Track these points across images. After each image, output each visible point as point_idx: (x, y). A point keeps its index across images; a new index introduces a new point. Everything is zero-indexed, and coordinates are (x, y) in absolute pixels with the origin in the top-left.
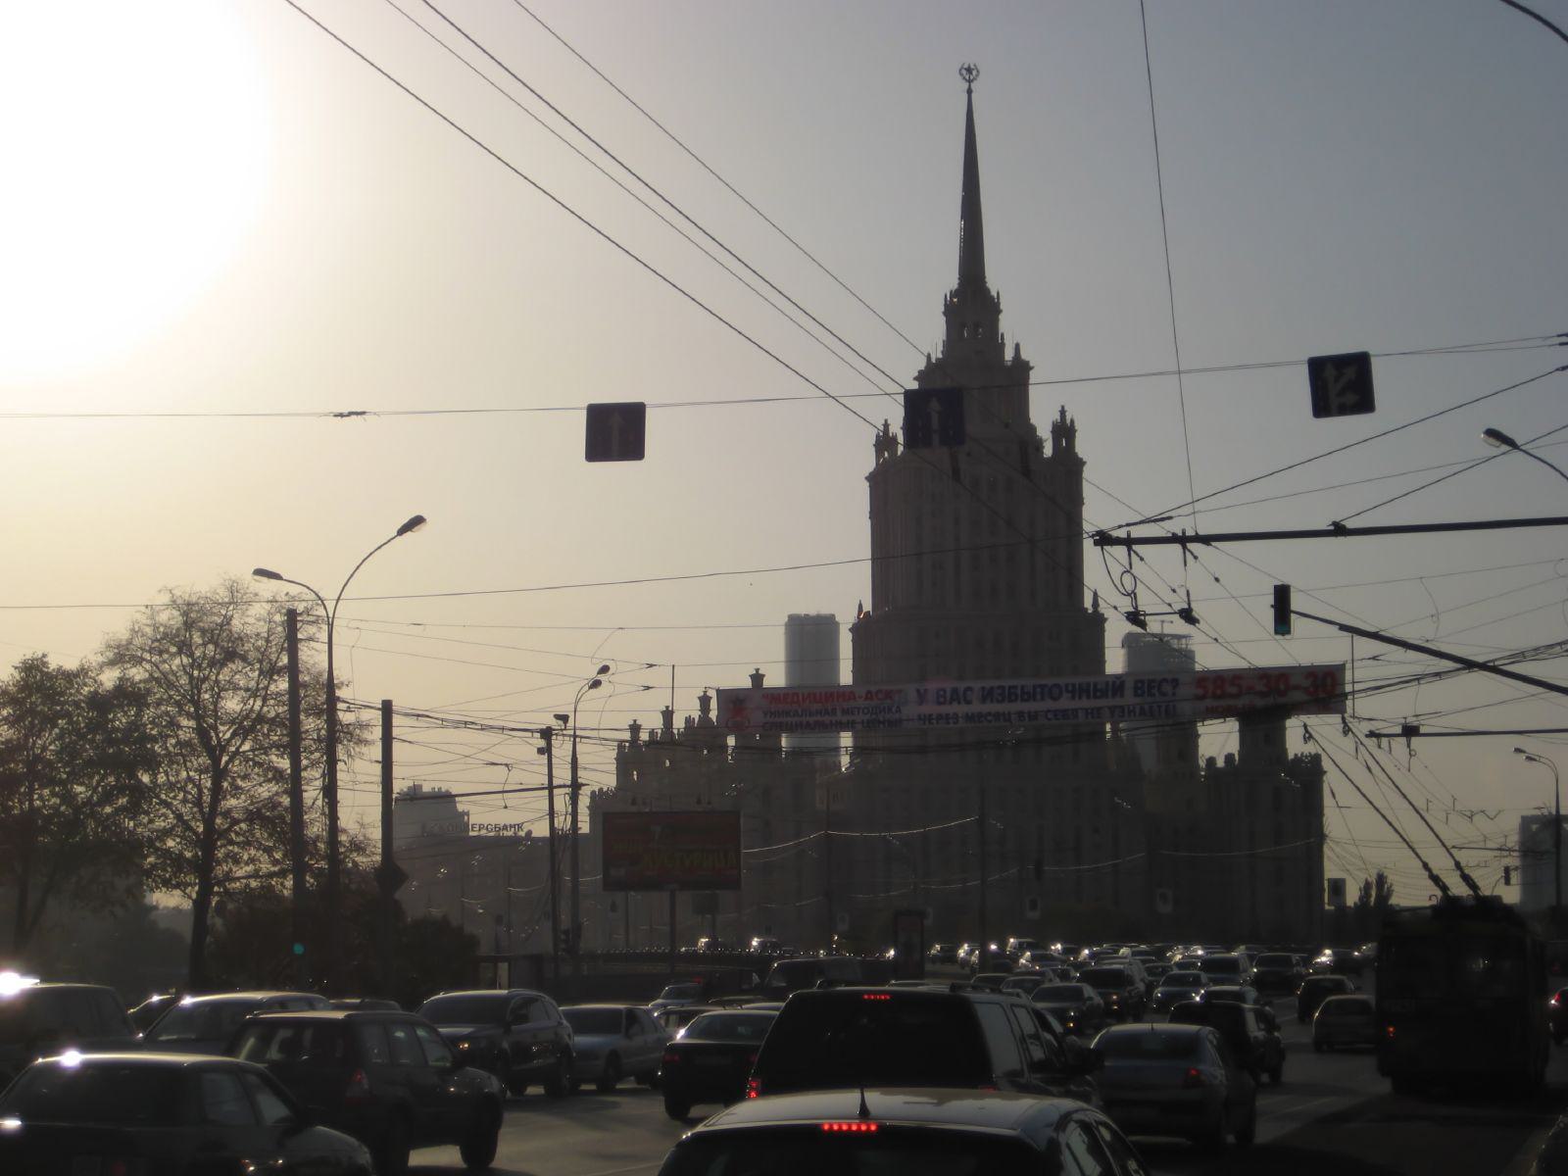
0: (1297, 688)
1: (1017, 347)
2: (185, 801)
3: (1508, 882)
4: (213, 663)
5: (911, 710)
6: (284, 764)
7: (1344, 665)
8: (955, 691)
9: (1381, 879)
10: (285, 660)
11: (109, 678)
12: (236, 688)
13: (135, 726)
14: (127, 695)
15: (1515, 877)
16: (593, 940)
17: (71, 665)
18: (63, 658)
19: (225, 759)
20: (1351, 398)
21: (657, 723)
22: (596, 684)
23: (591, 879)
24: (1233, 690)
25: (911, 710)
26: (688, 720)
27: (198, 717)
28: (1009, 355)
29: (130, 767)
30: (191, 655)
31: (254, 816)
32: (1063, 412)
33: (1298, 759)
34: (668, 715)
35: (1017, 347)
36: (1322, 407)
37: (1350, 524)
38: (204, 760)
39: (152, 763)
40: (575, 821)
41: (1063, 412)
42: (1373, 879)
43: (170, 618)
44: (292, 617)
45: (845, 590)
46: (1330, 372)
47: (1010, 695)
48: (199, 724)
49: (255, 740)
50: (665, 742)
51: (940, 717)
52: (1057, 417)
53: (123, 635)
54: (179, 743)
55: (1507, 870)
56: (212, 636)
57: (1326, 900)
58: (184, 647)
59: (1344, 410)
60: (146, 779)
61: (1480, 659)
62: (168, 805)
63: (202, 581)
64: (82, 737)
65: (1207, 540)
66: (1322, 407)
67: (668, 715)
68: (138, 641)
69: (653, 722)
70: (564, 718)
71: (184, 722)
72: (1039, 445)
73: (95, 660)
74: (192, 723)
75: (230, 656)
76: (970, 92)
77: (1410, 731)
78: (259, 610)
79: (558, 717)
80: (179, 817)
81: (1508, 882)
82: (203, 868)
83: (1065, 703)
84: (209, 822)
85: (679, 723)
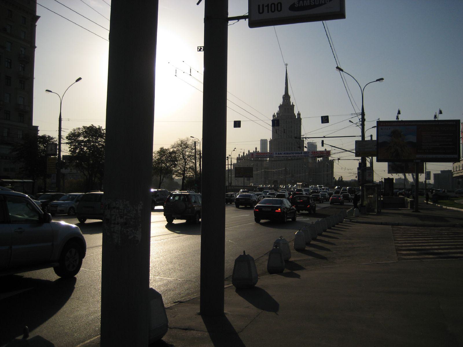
0: (325, 153)
1: (293, 103)
2: (181, 166)
3: (356, 178)
4: (185, 148)
5: (275, 155)
6: (194, 161)
7: (330, 151)
8: (280, 153)
9: (341, 177)
10: (194, 148)
11: (171, 150)
12: (188, 151)
13: (175, 156)
14: (174, 152)
15: (357, 177)
16: (233, 184)
17: (167, 148)
18: (166, 147)
19: (186, 160)
20: (326, 121)
21: (242, 155)
22: (234, 150)
23: (233, 176)
24: (316, 153)
25: (275, 155)
26: (247, 154)
27: (183, 155)
28: (291, 104)
29: (174, 161)
30: (182, 147)
31: (190, 168)
32: (299, 112)
33: (330, 160)
34: (244, 153)
35: (293, 103)
36: (323, 122)
37: (326, 136)
38: (184, 161)
39: (177, 161)
40: (231, 168)
41: (299, 112)
42: (340, 177)
43: (180, 142)
44: (195, 142)
45: (268, 135)
46: (324, 118)
47: (288, 154)
48: (183, 156)
49: (190, 158)
50: (243, 157)
51: (278, 156)
52: (298, 112)
53: (173, 144)
54: (180, 159)
55: (356, 176)
56: (185, 145)
57: (81, 233)
58: (181, 146)
59: (325, 123)
60: (176, 163)
61: (348, 150)
62: (179, 166)
63: (184, 138)
64: (168, 157)
65: (308, 138)
66: (323, 122)
67: (244, 153)
68: (175, 145)
69: (242, 154)
70: (230, 155)
71: (181, 156)
72: (296, 116)
73: (170, 148)
74: (182, 156)
75: (187, 147)
76: (286, 67)
77: (339, 159)
78: (191, 141)
79: (229, 155)
80: (180, 168)
81: (356, 178)
82: (184, 174)
83: (295, 155)
84: (184, 169)
85: (245, 154)
